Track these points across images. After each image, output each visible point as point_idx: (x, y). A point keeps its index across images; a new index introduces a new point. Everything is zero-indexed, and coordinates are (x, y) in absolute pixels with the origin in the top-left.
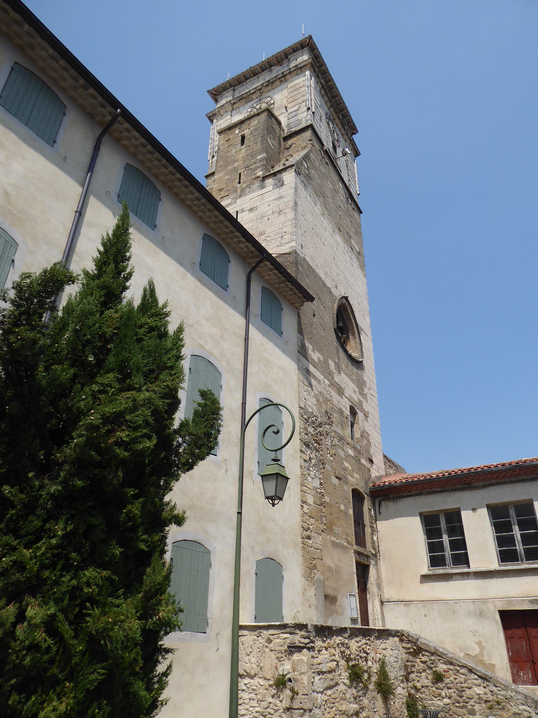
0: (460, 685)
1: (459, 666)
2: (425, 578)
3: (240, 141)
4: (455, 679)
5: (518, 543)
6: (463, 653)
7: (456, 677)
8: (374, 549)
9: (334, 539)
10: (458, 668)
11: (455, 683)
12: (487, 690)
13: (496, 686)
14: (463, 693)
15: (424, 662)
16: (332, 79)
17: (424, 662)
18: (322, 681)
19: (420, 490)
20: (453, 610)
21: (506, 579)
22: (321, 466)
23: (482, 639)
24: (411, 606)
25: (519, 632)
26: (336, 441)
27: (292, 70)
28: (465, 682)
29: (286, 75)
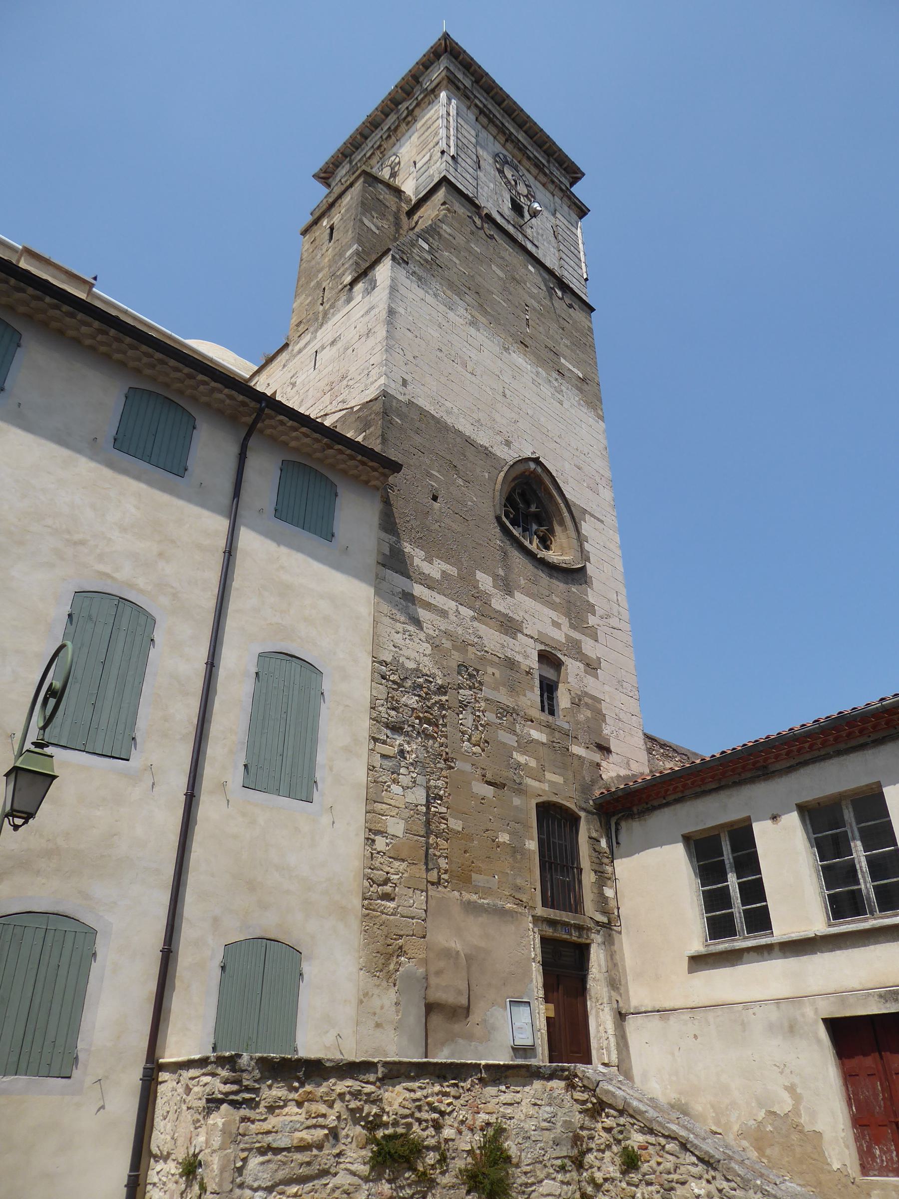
0: (666, 1176)
1: (664, 1136)
2: (698, 962)
3: (327, 237)
4: (659, 1164)
5: (864, 877)
6: (764, 1111)
7: (660, 1160)
8: (605, 912)
9: (474, 897)
10: (663, 1141)
11: (658, 1173)
12: (712, 1188)
13: (728, 1180)
14: (672, 1193)
15: (608, 1130)
16: (508, 96)
17: (608, 1130)
18: (272, 1166)
19: (682, 792)
20: (743, 1024)
21: (838, 952)
22: (442, 765)
23: (796, 1080)
24: (672, 1018)
25: (869, 1062)
26: (490, 717)
27: (419, 98)
28: (675, 1171)
29: (413, 110)
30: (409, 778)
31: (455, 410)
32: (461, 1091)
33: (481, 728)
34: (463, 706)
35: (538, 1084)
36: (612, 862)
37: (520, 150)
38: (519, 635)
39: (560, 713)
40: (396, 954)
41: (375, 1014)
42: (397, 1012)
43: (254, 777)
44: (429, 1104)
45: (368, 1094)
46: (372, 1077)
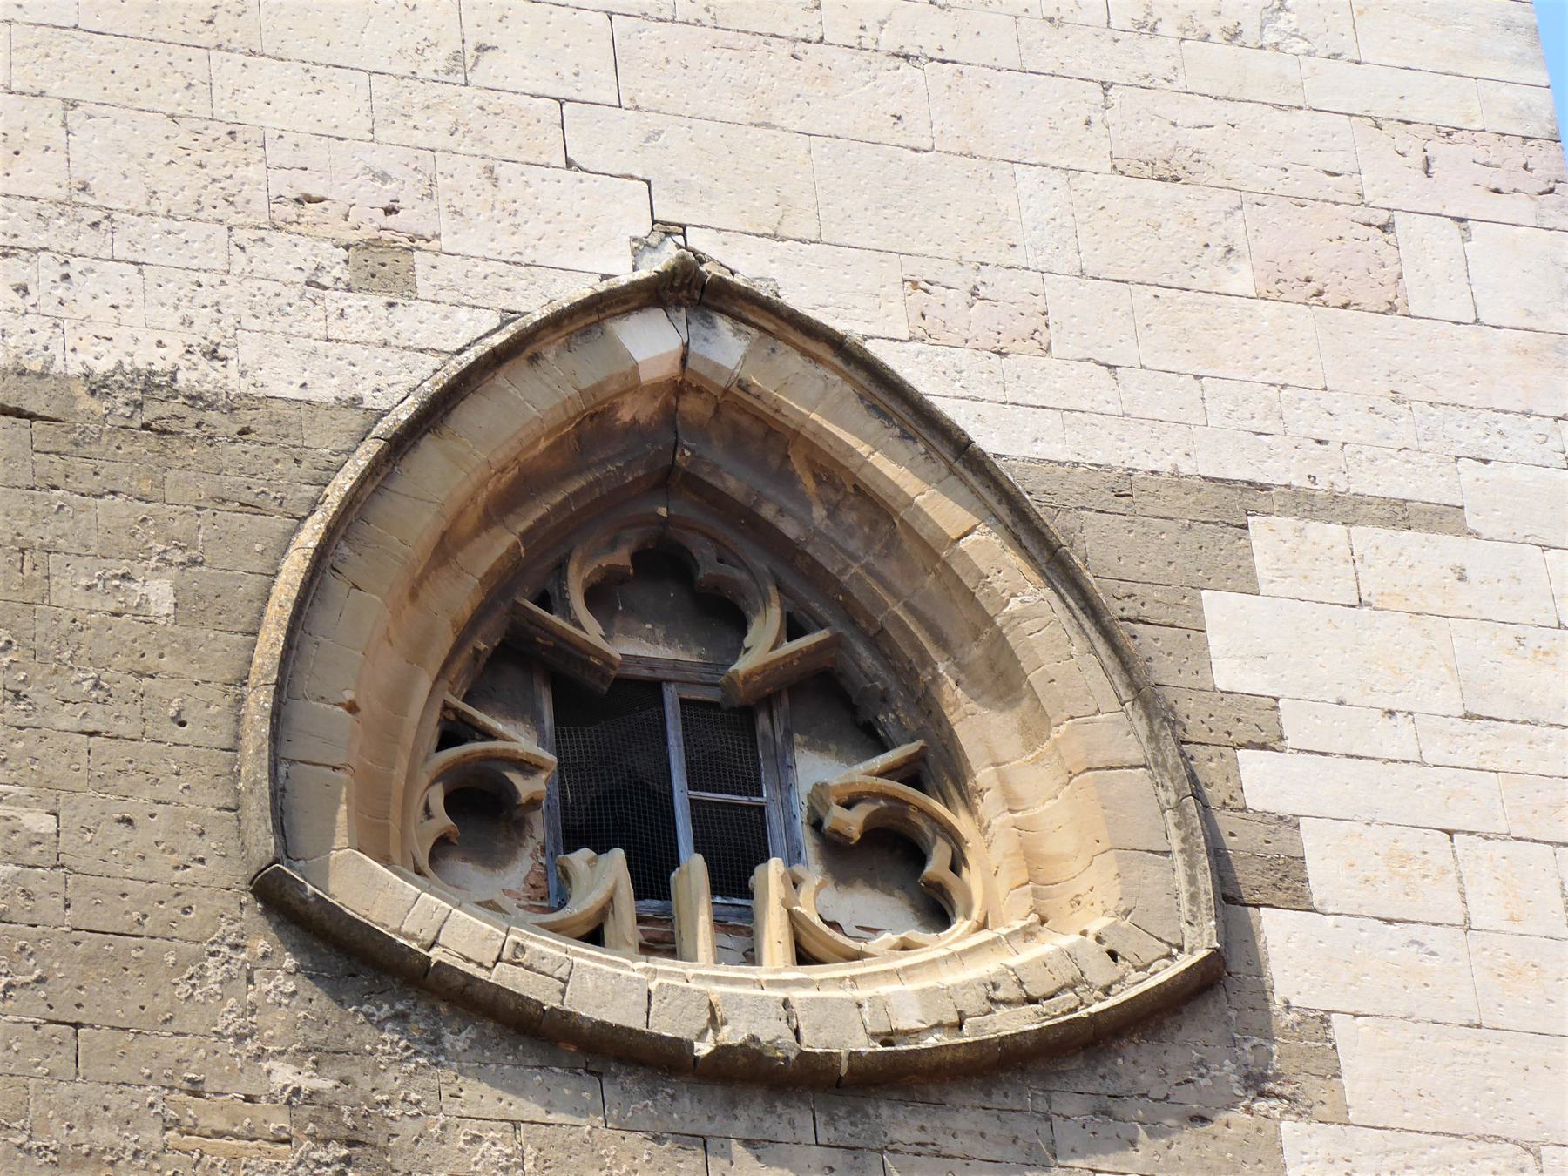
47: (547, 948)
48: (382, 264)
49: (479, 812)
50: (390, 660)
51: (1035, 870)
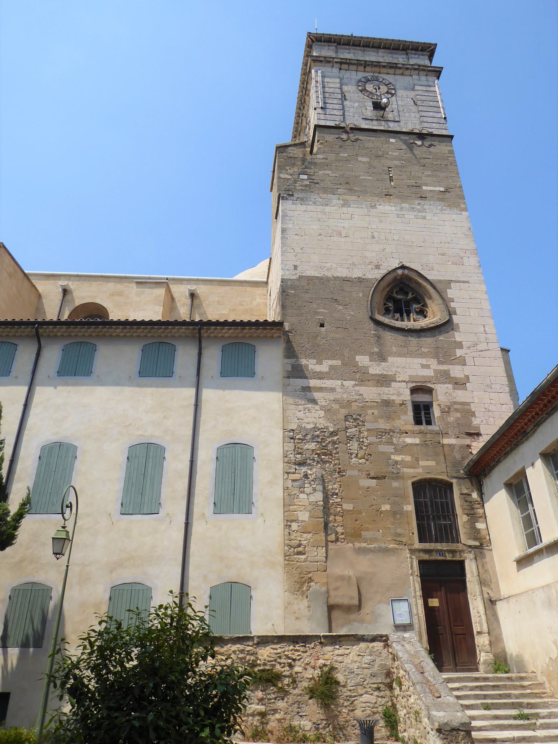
8: (475, 539)
9: (364, 545)
22: (337, 475)
30: (311, 488)
31: (334, 266)
32: (308, 649)
33: (364, 448)
34: (350, 438)
35: (363, 645)
36: (483, 506)
37: (376, 66)
38: (393, 384)
39: (436, 420)
40: (307, 582)
41: (295, 613)
42: (309, 611)
43: (219, 508)
44: (285, 655)
45: (248, 651)
46: (251, 643)
47: (393, 321)
48: (378, 267)
49: (387, 311)
50: (380, 299)
51: (433, 313)
